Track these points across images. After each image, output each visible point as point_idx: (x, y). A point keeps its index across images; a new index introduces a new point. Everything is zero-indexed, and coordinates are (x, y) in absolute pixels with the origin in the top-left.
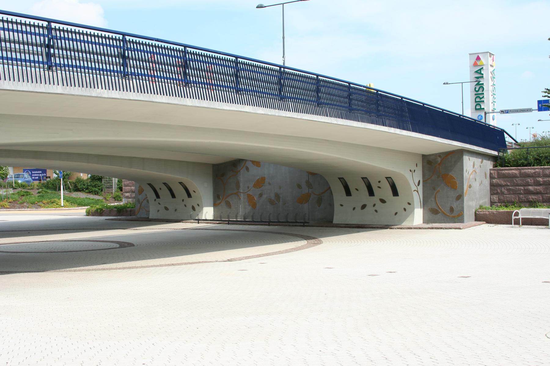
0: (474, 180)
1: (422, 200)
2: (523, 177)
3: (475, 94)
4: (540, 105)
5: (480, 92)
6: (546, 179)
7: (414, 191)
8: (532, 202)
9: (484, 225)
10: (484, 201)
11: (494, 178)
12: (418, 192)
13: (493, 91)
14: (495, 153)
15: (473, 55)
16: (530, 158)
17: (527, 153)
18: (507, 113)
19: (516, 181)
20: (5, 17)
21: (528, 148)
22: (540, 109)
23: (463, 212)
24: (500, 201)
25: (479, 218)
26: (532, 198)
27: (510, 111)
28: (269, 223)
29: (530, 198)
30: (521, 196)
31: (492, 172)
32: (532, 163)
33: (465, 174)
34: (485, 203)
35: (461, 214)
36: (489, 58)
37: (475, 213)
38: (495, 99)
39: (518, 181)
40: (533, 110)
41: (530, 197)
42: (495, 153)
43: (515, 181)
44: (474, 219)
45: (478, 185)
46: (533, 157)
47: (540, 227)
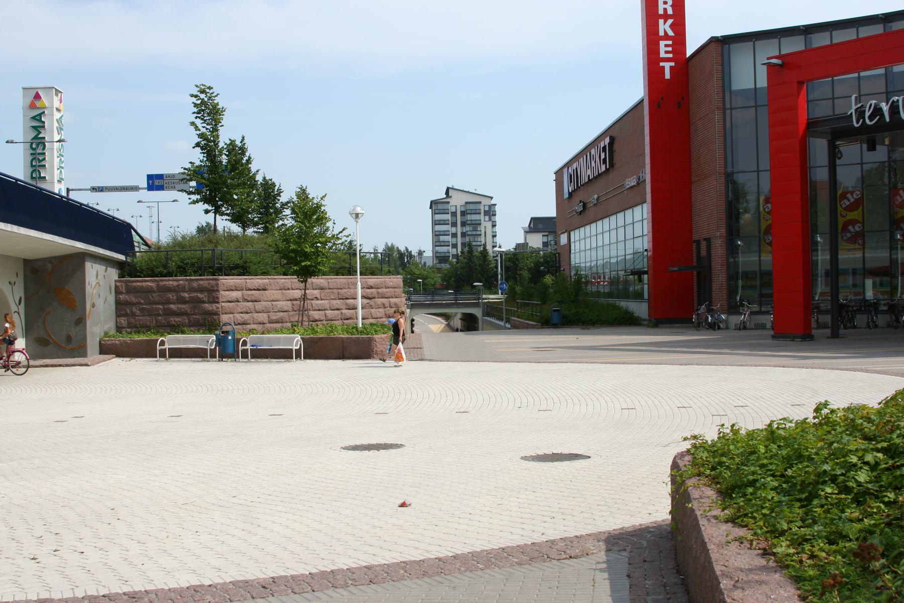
0: (97, 296)
1: (24, 329)
2: (162, 292)
3: (31, 154)
4: (151, 182)
5: (39, 151)
6: (193, 295)
7: (15, 312)
8: (174, 326)
9: (114, 359)
10: (109, 326)
11: (122, 293)
12: (19, 313)
13: (60, 150)
14: (122, 257)
16: (172, 265)
17: (167, 259)
18: (102, 191)
19: (153, 297)
21: (167, 252)
22: (150, 188)
23: (86, 342)
24: (130, 325)
25: (107, 349)
26: (175, 321)
27: (106, 189)
29: (171, 321)
30: (160, 318)
31: (118, 284)
32: (173, 272)
33: (88, 288)
34: (110, 328)
35: (83, 344)
36: (55, 97)
37: (100, 342)
38: (63, 162)
39: (156, 297)
40: (140, 189)
41: (172, 319)
42: (122, 257)
43: (150, 297)
44: (98, 352)
45: (102, 303)
46: (176, 264)
47: (193, 359)
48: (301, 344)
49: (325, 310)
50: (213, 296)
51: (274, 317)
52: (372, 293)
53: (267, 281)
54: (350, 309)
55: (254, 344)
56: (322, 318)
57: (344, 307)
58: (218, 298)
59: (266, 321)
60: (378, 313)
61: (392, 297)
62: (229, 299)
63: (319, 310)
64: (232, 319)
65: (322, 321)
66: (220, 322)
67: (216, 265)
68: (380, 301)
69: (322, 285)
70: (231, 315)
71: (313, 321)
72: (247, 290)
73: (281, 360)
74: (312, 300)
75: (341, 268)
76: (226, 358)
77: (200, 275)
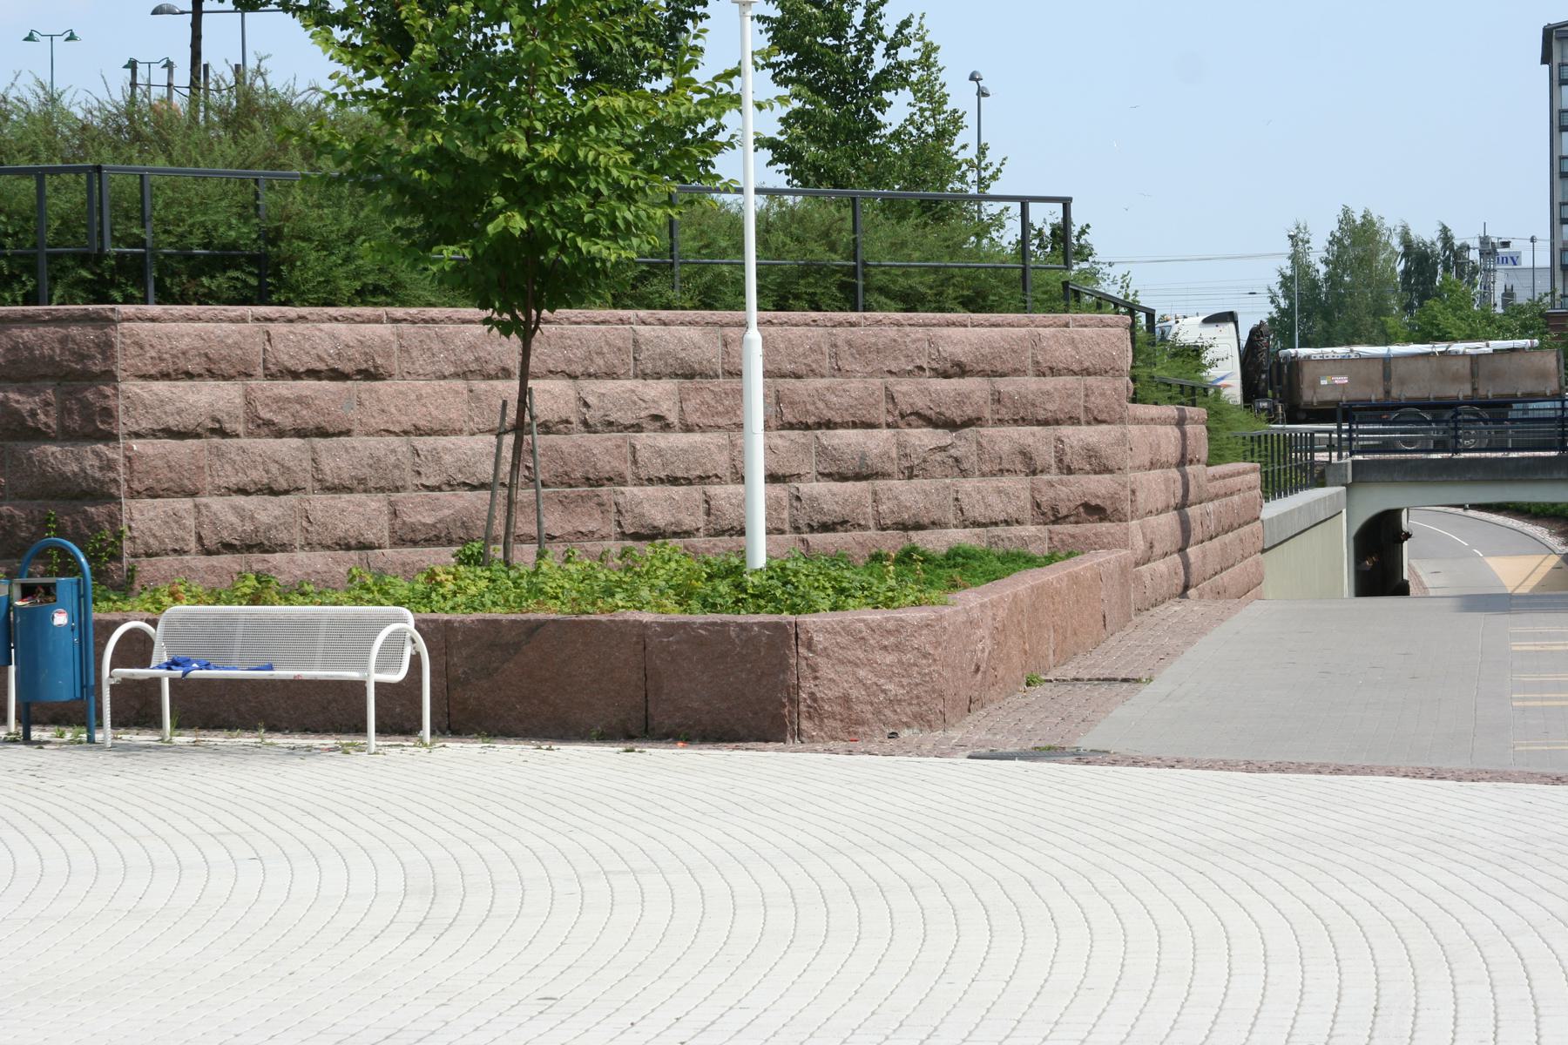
48: (416, 661)
49: (703, 479)
50: (86, 406)
51: (421, 511)
52: (962, 399)
53: (385, 330)
54: (843, 478)
55: (181, 655)
56: (688, 522)
57: (809, 467)
58: (108, 414)
59: (379, 530)
60: (993, 499)
61: (1074, 421)
62: (172, 422)
63: (674, 481)
64: (190, 522)
65: (688, 534)
66: (119, 536)
67: (111, 249)
68: (1006, 438)
69: (693, 358)
70: (183, 504)
71: (637, 537)
72: (271, 376)
73: (315, 741)
74: (638, 428)
75: (806, 271)
76: (44, 723)
77: (29, 299)
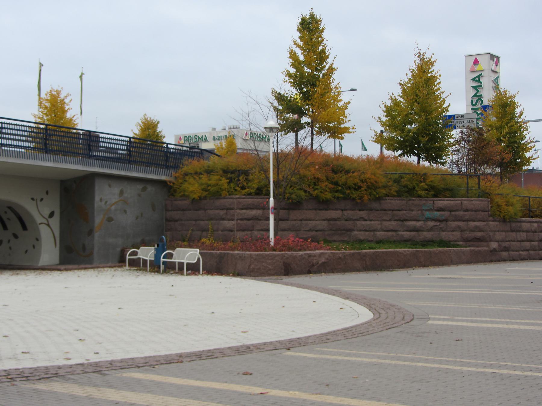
15: (484, 55)
20: (3, 121)
28: (167, 146)
68: (454, 224)
